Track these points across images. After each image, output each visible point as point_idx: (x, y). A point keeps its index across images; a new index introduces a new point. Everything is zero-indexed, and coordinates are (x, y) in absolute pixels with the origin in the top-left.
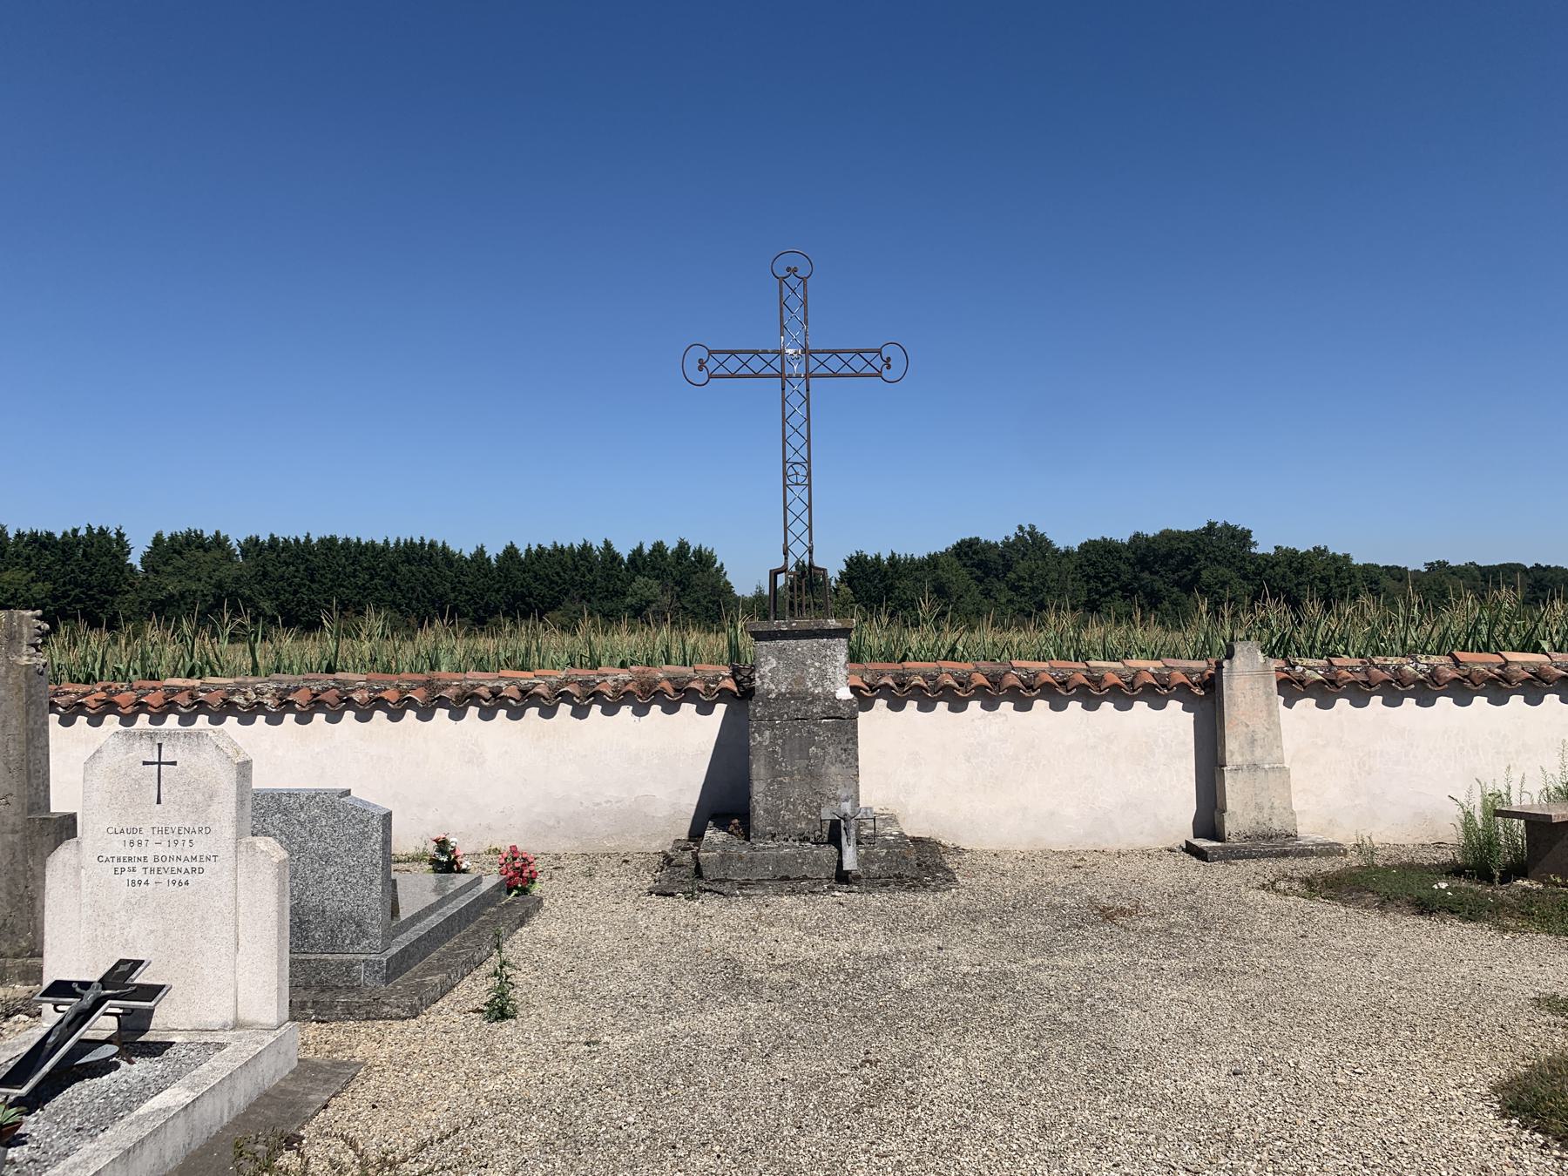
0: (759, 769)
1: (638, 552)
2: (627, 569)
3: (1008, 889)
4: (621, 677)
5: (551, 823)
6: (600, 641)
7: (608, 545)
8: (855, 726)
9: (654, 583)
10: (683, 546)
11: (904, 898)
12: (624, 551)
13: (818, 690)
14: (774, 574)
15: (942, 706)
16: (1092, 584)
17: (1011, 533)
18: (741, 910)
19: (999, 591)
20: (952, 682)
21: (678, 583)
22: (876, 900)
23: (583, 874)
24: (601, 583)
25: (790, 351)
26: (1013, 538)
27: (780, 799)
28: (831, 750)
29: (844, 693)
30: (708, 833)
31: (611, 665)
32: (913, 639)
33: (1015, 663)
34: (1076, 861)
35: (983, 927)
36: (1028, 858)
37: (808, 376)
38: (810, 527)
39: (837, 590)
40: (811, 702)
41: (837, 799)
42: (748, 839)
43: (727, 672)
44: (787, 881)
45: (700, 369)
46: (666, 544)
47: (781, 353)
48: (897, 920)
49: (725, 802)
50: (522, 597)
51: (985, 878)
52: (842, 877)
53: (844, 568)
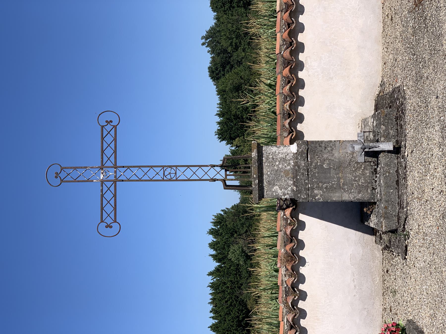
0: (336, 197)
1: (215, 257)
2: (224, 263)
3: (404, 58)
4: (283, 273)
5: (366, 313)
6: (265, 282)
7: (210, 274)
8: (312, 142)
9: (232, 248)
10: (212, 232)
11: (408, 116)
12: (214, 265)
14: (227, 187)
15: (301, 93)
16: (235, 5)
17: (206, 49)
18: (415, 209)
19: (238, 56)
20: (288, 87)
21: (232, 235)
22: (410, 132)
23: (394, 296)
24: (231, 278)
25: (102, 177)
26: (209, 49)
27: (352, 185)
28: (325, 156)
29: (294, 148)
30: (372, 225)
31: (276, 277)
32: (263, 107)
33: (277, 51)
34: (389, 20)
35: (425, 73)
36: (387, 45)
37: (115, 166)
38: (200, 166)
39: (237, 146)
40: (299, 167)
41: (353, 153)
42: (375, 203)
43: (281, 213)
44: (399, 181)
45: (111, 227)
46: (210, 241)
47: (102, 182)
48: (421, 121)
49: (355, 215)
50: (239, 321)
51: (398, 70)
52: (397, 150)
53: (224, 142)
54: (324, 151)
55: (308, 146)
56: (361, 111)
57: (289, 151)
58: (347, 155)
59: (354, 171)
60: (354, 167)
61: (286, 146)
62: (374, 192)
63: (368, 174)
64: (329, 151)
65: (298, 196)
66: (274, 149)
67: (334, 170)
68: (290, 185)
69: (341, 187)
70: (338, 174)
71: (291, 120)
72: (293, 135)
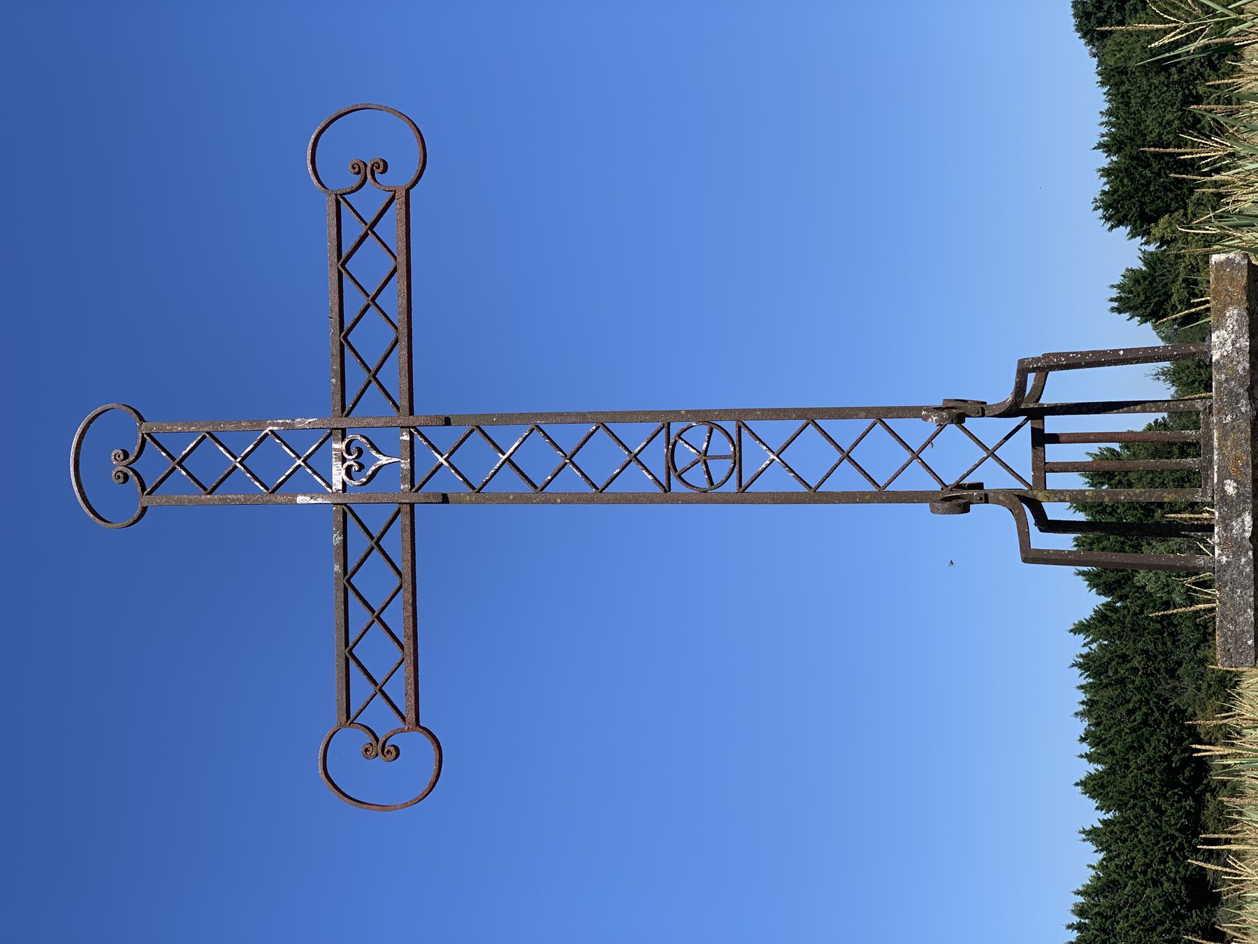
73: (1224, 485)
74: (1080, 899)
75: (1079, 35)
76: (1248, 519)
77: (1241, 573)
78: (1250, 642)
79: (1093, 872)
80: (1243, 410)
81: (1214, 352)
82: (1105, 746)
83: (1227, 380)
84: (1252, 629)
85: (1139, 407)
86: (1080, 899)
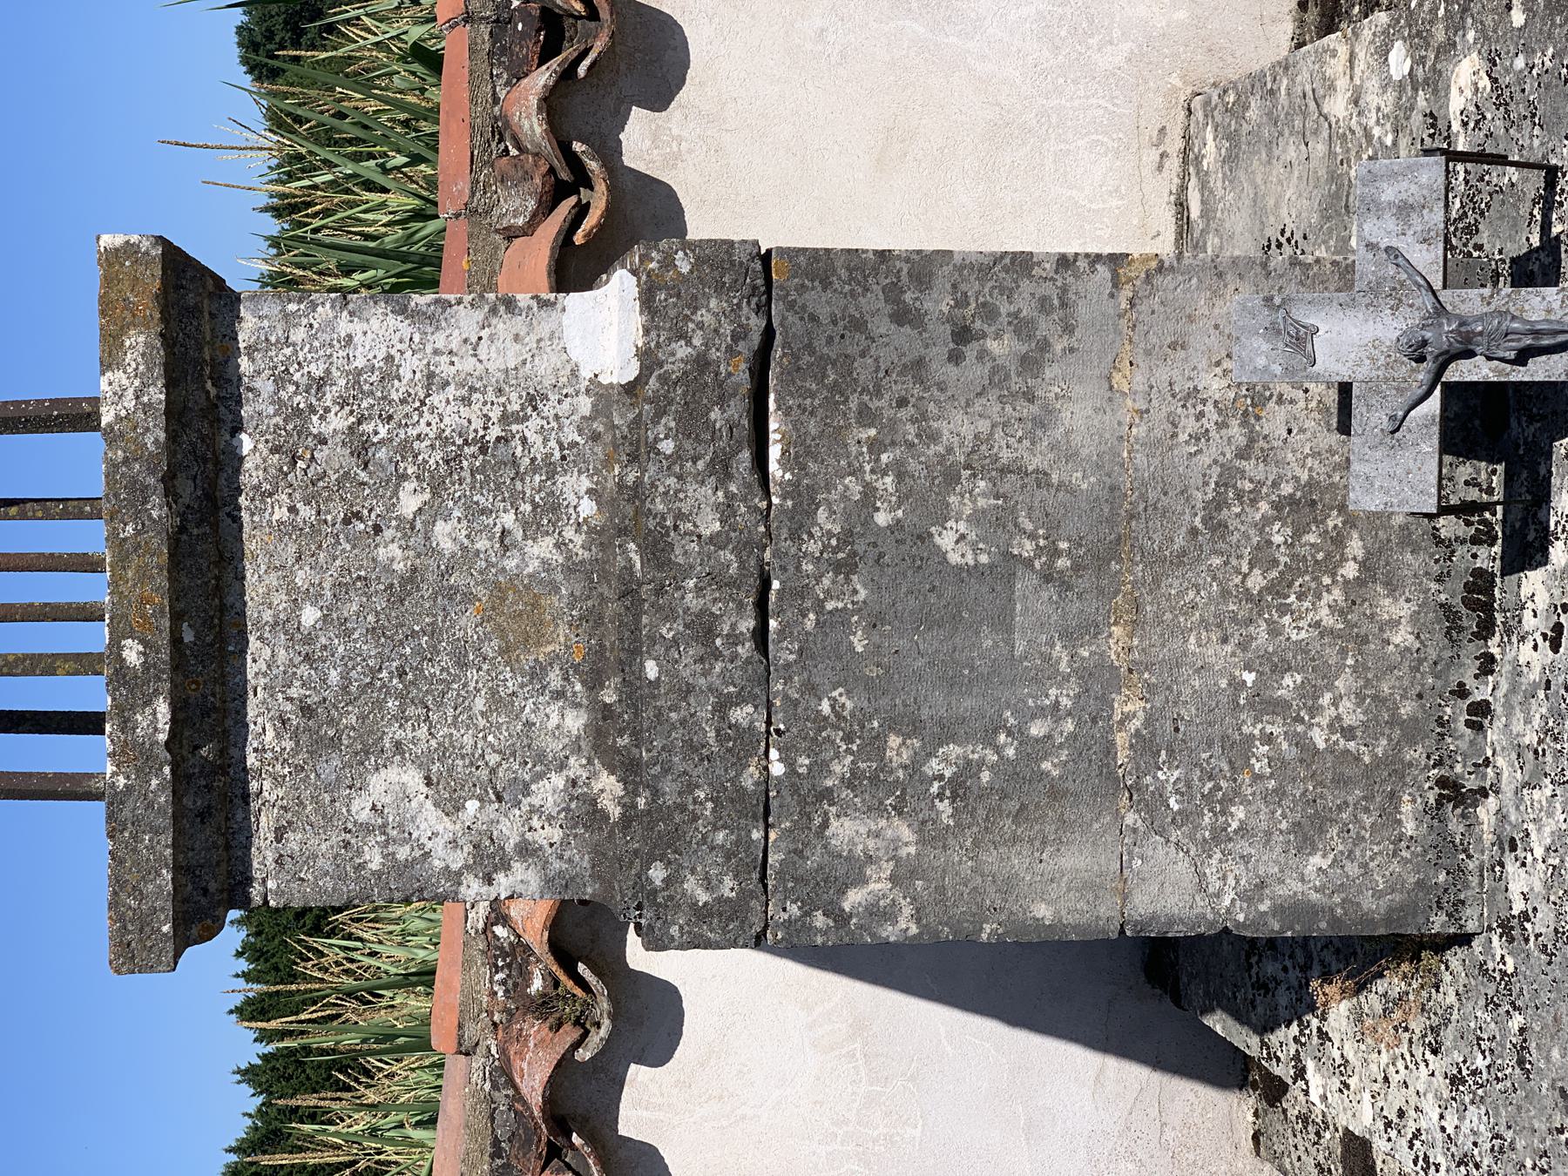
8: (819, 266)
13: (579, 495)
27: (1238, 752)
28: (958, 428)
29: (603, 329)
40: (657, 549)
54: (942, 370)
55: (765, 309)
56: (1182, 15)
57: (545, 368)
58: (1189, 425)
59: (1257, 601)
60: (1263, 556)
61: (510, 304)
62: (1455, 826)
63: (1402, 637)
64: (998, 376)
65: (641, 881)
66: (375, 332)
67: (1050, 592)
68: (554, 746)
69: (1111, 780)
70: (1093, 629)
71: (568, 73)
72: (582, 210)
73: (121, 648)
74: (233, 1158)
75: (244, 69)
76: (163, 709)
77: (150, 806)
78: (165, 929)
79: (249, 1122)
80: (155, 514)
81: (103, 410)
82: (267, 961)
83: (126, 461)
84: (169, 905)
85: (13, 510)
86: (233, 1158)
